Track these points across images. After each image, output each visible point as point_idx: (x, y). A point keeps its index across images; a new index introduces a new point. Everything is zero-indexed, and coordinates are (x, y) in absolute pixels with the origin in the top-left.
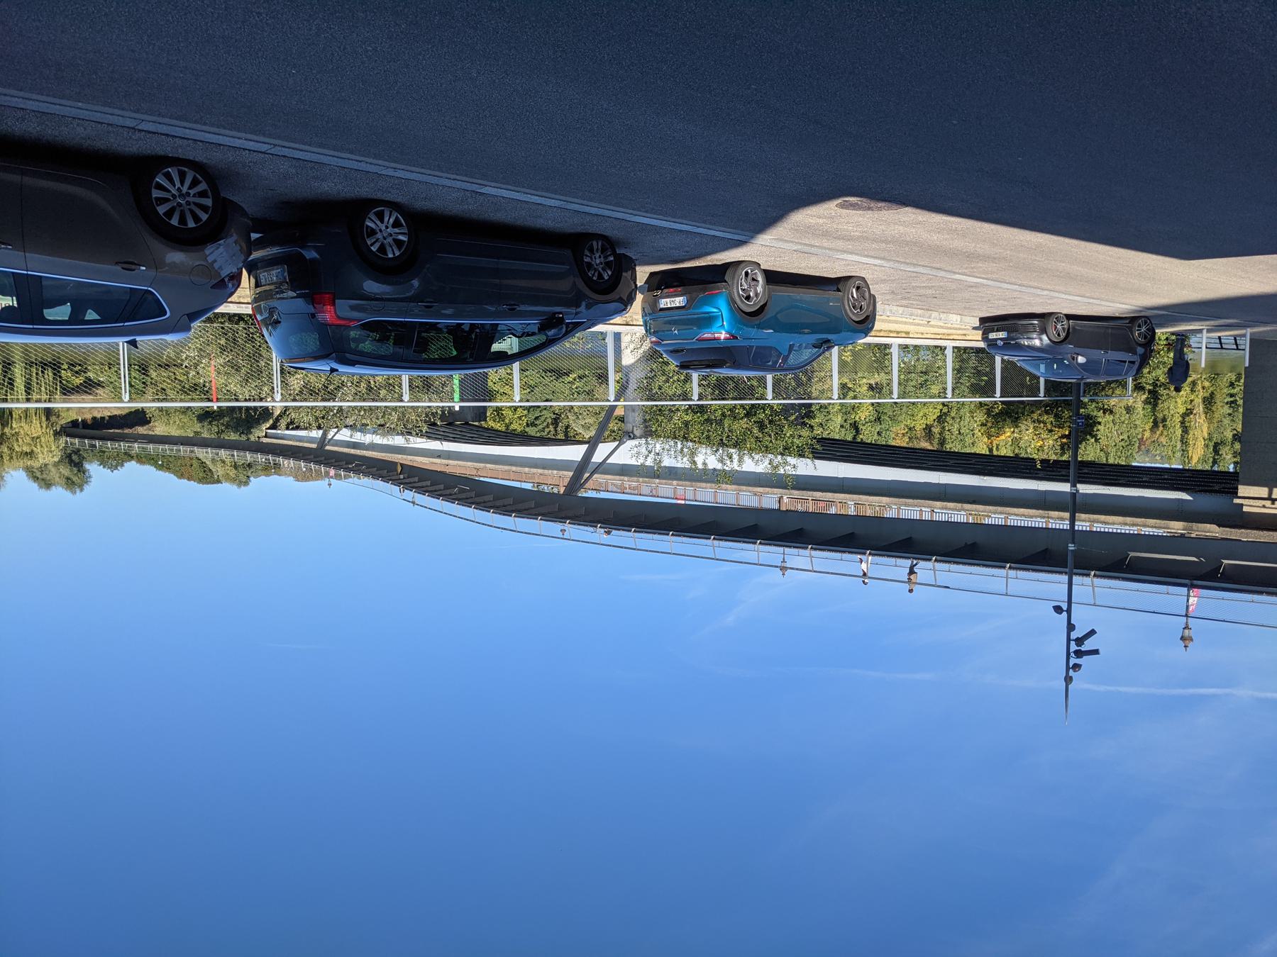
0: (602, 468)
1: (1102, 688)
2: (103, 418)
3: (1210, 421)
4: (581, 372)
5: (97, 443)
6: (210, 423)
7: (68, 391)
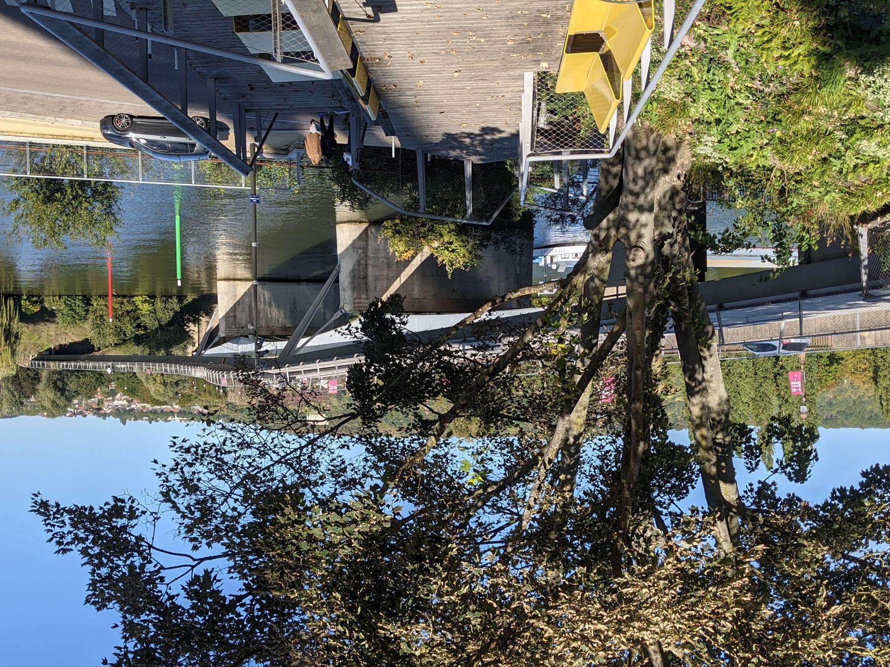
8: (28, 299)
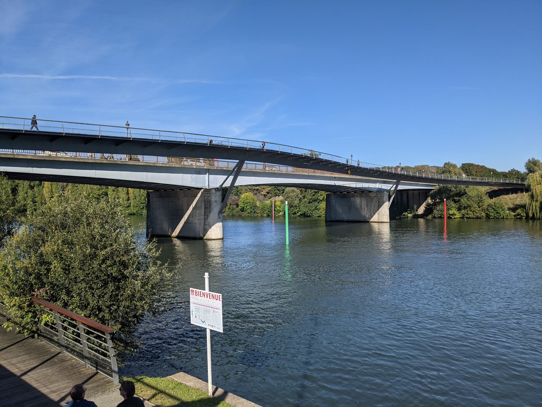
0: (227, 173)
1: (106, 77)
2: (512, 193)
3: (42, 195)
4: (295, 216)
5: (520, 182)
6: (460, 192)
7: (523, 206)
8: (522, 216)
